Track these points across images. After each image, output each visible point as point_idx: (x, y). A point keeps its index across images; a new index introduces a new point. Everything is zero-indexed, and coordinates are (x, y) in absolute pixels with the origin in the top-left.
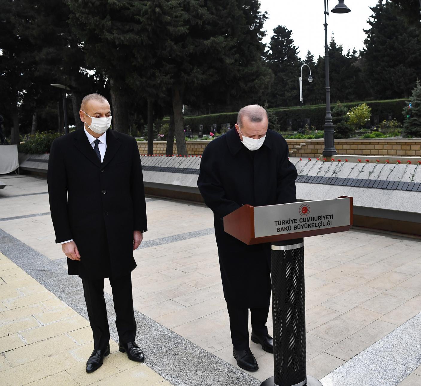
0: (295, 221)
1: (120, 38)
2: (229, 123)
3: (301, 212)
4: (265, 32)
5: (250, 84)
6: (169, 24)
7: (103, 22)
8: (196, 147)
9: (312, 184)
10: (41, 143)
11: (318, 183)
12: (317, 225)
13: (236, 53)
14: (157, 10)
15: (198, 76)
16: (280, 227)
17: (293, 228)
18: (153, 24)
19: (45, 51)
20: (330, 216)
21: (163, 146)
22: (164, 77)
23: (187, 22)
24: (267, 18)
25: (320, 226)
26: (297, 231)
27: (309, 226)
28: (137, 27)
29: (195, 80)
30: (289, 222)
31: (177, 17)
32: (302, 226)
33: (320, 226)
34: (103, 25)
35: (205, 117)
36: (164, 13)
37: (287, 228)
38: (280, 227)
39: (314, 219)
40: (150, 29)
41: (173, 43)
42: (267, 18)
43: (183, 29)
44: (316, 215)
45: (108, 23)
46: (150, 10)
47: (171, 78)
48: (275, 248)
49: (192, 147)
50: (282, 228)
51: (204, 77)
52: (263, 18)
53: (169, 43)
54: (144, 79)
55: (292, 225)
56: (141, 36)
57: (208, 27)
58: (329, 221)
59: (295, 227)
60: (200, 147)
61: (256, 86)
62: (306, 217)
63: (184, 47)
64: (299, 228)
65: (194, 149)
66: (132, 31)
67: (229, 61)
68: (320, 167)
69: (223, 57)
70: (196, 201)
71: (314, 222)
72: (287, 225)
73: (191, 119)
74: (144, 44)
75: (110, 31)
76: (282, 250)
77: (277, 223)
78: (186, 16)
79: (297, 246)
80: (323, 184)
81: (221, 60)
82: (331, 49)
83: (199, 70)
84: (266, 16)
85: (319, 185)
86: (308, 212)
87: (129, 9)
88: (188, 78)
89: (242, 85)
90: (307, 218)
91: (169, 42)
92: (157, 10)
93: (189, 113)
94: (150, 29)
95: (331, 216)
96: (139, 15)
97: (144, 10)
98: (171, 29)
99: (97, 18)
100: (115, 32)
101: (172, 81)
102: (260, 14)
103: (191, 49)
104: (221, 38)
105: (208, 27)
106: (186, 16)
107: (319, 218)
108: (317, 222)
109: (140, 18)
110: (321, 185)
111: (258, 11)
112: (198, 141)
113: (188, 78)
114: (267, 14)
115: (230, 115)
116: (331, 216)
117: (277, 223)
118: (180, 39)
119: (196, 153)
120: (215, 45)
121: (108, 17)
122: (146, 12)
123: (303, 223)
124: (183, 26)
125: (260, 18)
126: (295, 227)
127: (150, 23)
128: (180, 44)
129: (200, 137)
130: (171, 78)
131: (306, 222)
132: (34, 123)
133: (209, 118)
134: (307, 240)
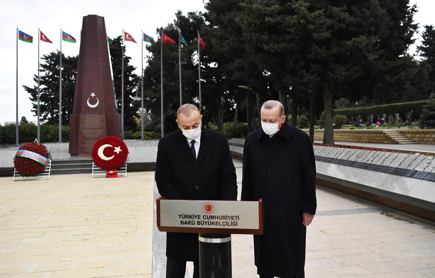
0: (199, 216)
1: (275, 48)
2: (398, 112)
3: (205, 210)
4: (417, 24)
5: (397, 77)
6: (314, 31)
7: (262, 36)
8: (360, 135)
9: (416, 180)
10: (230, 131)
11: (423, 179)
12: (221, 224)
13: (380, 48)
14: (302, 21)
15: (341, 72)
16: (184, 220)
17: (196, 223)
18: (300, 33)
19: (237, 61)
20: (236, 217)
21: (322, 134)
22: (310, 76)
23: (329, 28)
24: (416, 11)
25: (224, 226)
26: (200, 226)
27: (213, 223)
28: (288, 37)
29: (339, 76)
30: (192, 217)
31: (321, 24)
32: (206, 223)
33: (224, 226)
34: (262, 39)
35: (375, 108)
36: (308, 22)
37: (191, 223)
38: (184, 220)
39: (218, 217)
40: (298, 37)
41: (317, 47)
42: (416, 11)
43: (327, 34)
44: (220, 214)
45: (265, 37)
46: (297, 22)
47: (316, 77)
48: (201, 239)
49: (357, 135)
50: (186, 221)
51: (348, 73)
52: (412, 12)
53: (315, 47)
54: (296, 79)
55: (196, 220)
56: (291, 45)
57: (351, 29)
58: (234, 222)
59: (199, 223)
60: (364, 135)
61: (402, 78)
62: (210, 215)
63: (328, 49)
64: (202, 224)
65: (359, 137)
66: (284, 41)
67: (371, 57)
68: (429, 161)
69: (365, 54)
70: (322, 185)
71: (219, 220)
72: (191, 220)
73: (363, 110)
74: (294, 50)
75: (267, 43)
76: (219, 242)
77: (181, 216)
78: (329, 22)
79: (226, 240)
80: (427, 180)
81: (365, 57)
82: (73, 76)
83: (342, 68)
84: (416, 9)
85: (424, 181)
86: (212, 210)
87: (282, 24)
88: (333, 75)
89: (388, 78)
90: (211, 216)
91: (314, 46)
92: (302, 21)
93: (366, 104)
94: (298, 37)
95: (237, 218)
96: (290, 27)
97: (292, 23)
98: (315, 35)
99: (258, 34)
100: (270, 43)
101: (318, 79)
102: (408, 9)
103: (335, 50)
104: (362, 38)
105: (351, 29)
106: (329, 22)
107: (224, 217)
108: (221, 221)
109: (290, 29)
110: (426, 181)
111: (408, 5)
112: (365, 129)
113: (333, 75)
114: (416, 7)
115: (399, 105)
116: (237, 218)
117: (181, 216)
118: (322, 43)
119: (361, 140)
120: (356, 44)
121: (266, 32)
122: (294, 24)
123: (206, 220)
124: (326, 31)
125: (409, 12)
126: (199, 223)
127: (297, 32)
128: (324, 47)
129: (368, 126)
130: (316, 77)
131: (210, 219)
132: (236, 115)
133: (379, 108)
134: (234, 237)
